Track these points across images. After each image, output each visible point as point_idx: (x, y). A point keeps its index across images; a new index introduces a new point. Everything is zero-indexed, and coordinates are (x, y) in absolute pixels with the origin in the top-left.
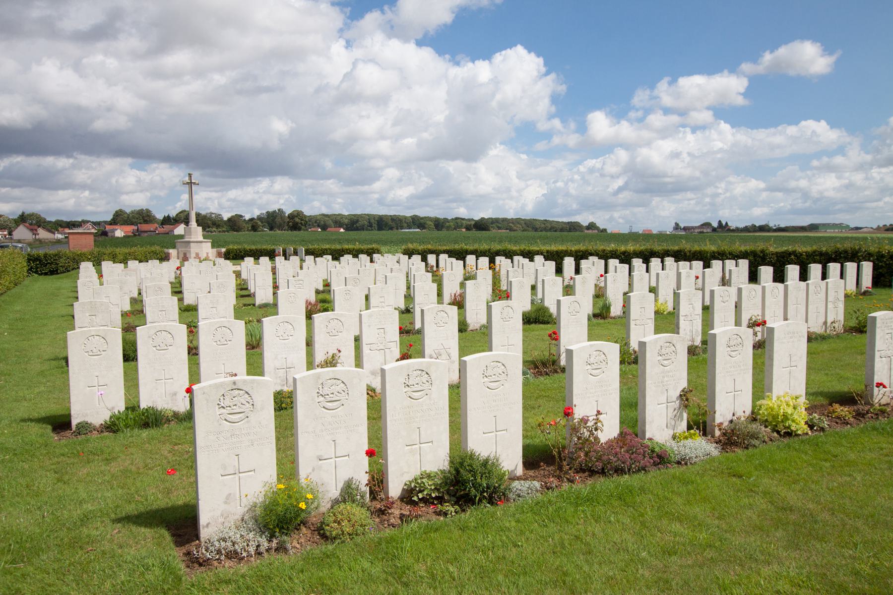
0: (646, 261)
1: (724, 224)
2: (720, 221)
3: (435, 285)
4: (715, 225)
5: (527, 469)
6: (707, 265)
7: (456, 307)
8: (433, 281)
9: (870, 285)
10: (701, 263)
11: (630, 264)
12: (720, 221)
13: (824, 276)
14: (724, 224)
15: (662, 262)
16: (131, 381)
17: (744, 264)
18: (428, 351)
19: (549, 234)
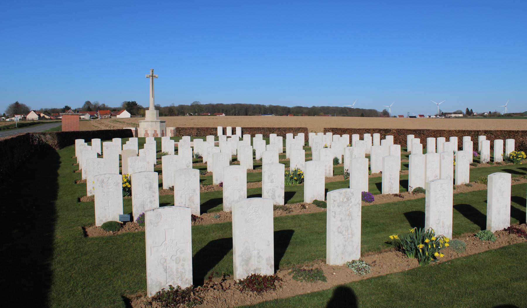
0: (266, 138)
1: (470, 110)
2: (467, 109)
3: (489, 142)
4: (465, 112)
5: (422, 210)
6: (448, 140)
7: (157, 173)
8: (395, 142)
9: (513, 150)
10: (445, 138)
11: (285, 138)
12: (467, 109)
13: (425, 150)
14: (470, 110)
15: (372, 136)
16: (149, 211)
17: (454, 140)
18: (176, 203)
19: (457, 115)
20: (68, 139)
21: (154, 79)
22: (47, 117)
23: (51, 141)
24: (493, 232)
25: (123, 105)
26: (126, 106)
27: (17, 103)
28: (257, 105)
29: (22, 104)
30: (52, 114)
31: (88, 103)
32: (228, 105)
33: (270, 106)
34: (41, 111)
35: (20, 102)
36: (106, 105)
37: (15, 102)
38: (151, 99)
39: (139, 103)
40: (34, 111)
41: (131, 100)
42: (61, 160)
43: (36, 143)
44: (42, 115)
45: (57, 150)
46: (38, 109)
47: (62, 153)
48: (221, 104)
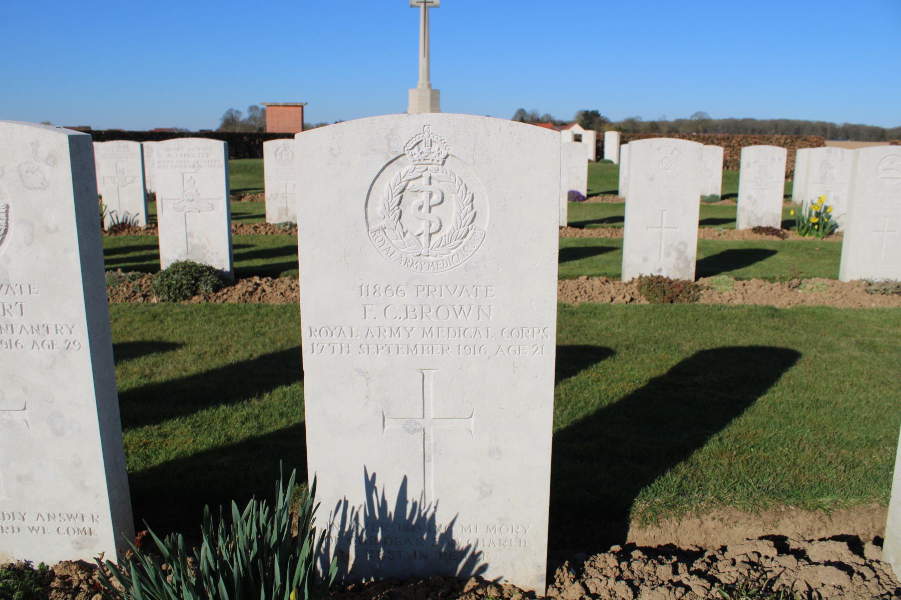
25: (578, 117)
26: (583, 118)
28: (820, 123)
32: (719, 120)
39: (603, 113)
41: (591, 108)
48: (752, 120)
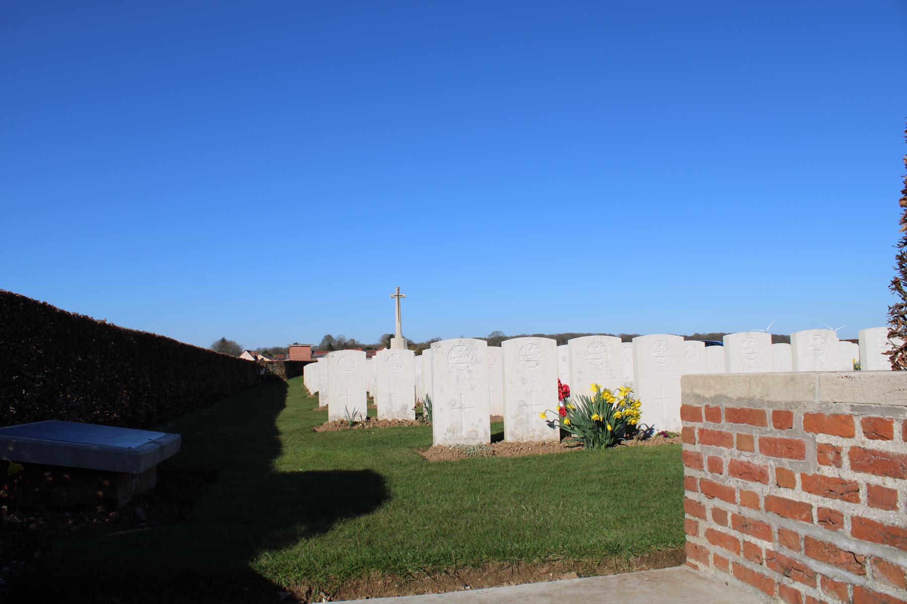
20: (296, 369)
21: (401, 299)
22: (266, 360)
23: (279, 371)
24: (675, 425)
25: (383, 341)
27: (223, 340)
29: (231, 342)
30: (275, 356)
31: (328, 338)
33: (45, 303)
34: (258, 352)
35: (228, 339)
36: (356, 340)
37: (220, 339)
38: (397, 324)
40: (249, 352)
42: (282, 438)
43: (262, 373)
44: (260, 357)
45: (285, 380)
46: (254, 349)
47: (290, 382)
